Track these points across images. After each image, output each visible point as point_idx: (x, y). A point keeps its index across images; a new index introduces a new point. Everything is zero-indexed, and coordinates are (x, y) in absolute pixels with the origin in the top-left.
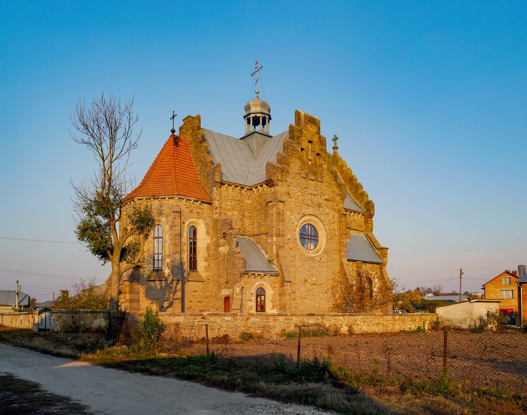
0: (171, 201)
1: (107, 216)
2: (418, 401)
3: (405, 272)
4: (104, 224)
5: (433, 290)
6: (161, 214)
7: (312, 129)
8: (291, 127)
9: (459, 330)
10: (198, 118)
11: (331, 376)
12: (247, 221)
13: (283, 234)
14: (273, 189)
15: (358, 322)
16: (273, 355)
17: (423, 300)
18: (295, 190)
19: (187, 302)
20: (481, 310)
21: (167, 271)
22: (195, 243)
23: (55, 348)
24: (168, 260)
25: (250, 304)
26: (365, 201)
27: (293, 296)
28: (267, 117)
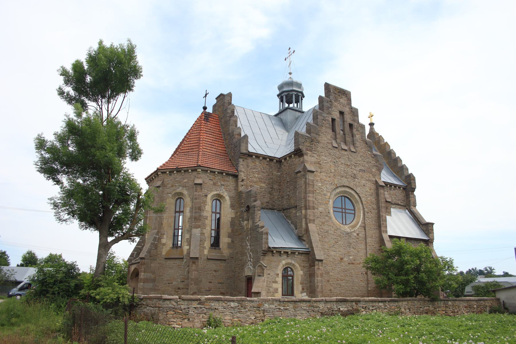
7: (343, 100)
10: (230, 95)
13: (314, 207)
15: (403, 310)
25: (275, 285)
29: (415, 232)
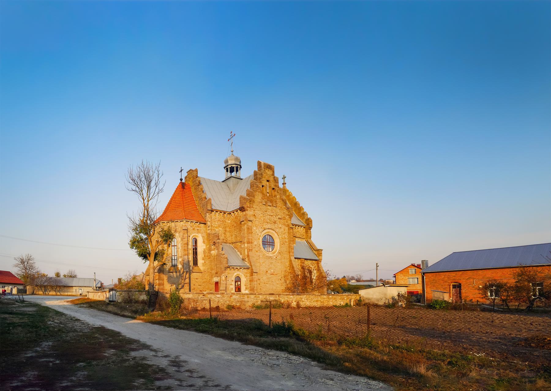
0: (182, 223)
1: (146, 234)
2: (351, 351)
3: (334, 266)
4: (147, 238)
5: (356, 278)
6: (176, 231)
7: (269, 172)
8: (255, 172)
9: (376, 306)
10: (196, 170)
11: (294, 333)
12: (228, 234)
14: (244, 213)
15: (303, 300)
16: (251, 319)
17: (349, 285)
18: (258, 213)
19: (192, 285)
20: (393, 292)
21: (180, 266)
22: (196, 249)
23: (121, 312)
24: (180, 260)
25: (231, 287)
26: (306, 218)
27: (258, 282)
28: (239, 166)
29: (310, 255)
